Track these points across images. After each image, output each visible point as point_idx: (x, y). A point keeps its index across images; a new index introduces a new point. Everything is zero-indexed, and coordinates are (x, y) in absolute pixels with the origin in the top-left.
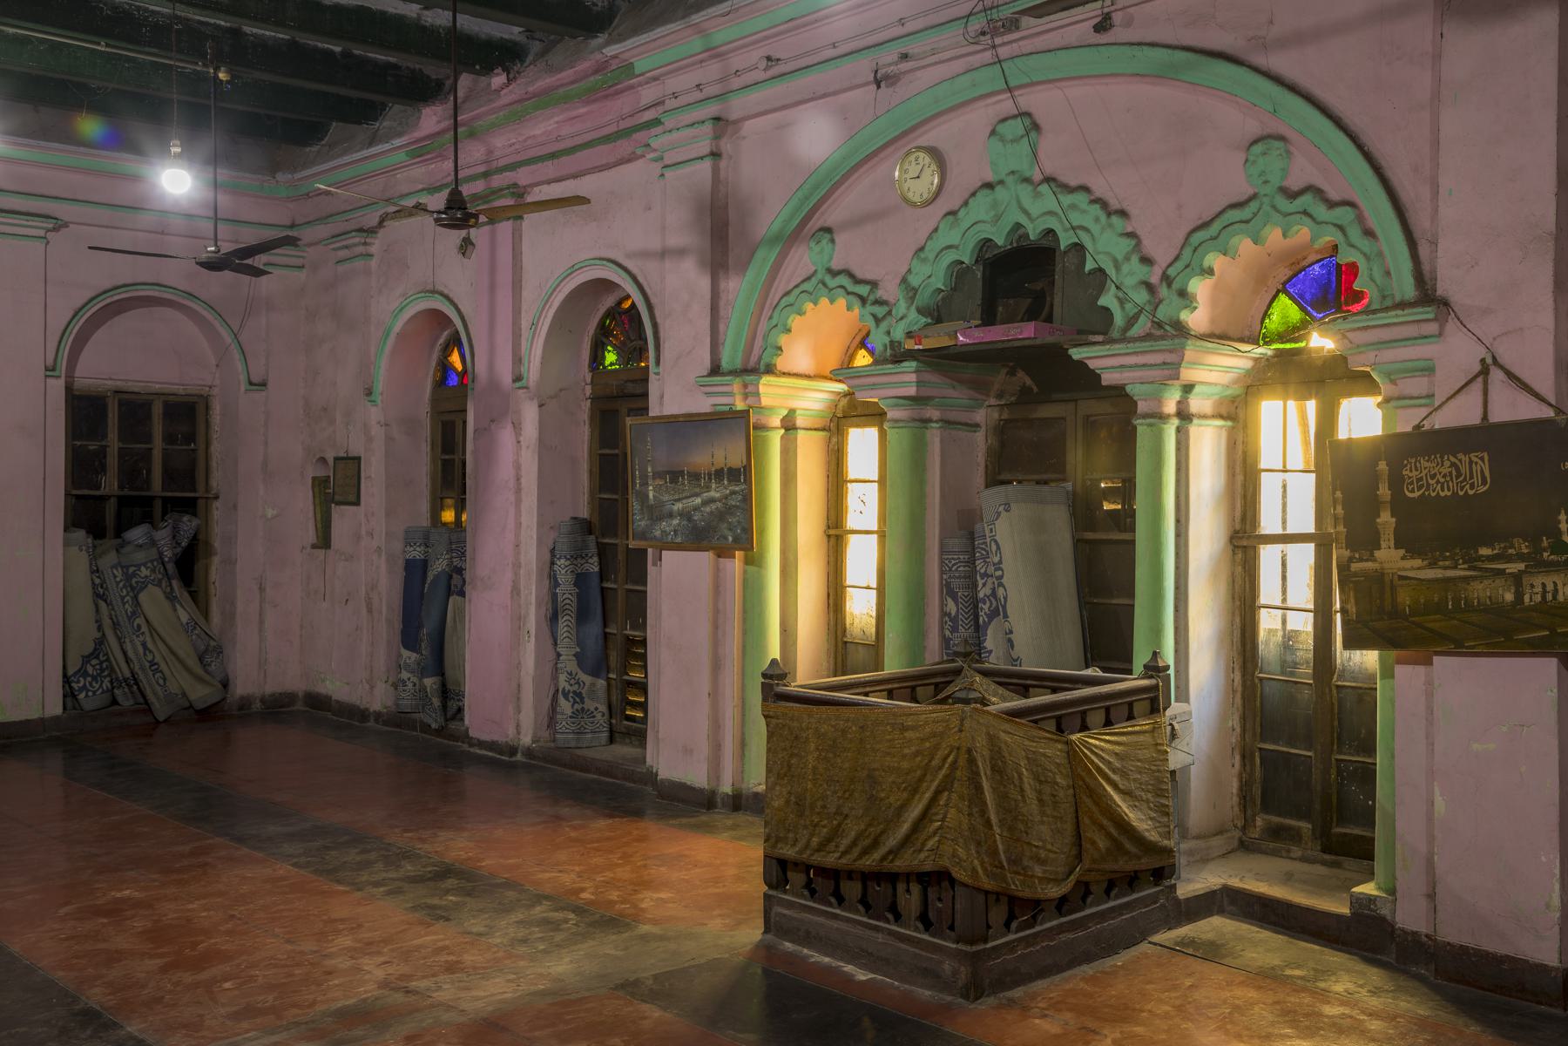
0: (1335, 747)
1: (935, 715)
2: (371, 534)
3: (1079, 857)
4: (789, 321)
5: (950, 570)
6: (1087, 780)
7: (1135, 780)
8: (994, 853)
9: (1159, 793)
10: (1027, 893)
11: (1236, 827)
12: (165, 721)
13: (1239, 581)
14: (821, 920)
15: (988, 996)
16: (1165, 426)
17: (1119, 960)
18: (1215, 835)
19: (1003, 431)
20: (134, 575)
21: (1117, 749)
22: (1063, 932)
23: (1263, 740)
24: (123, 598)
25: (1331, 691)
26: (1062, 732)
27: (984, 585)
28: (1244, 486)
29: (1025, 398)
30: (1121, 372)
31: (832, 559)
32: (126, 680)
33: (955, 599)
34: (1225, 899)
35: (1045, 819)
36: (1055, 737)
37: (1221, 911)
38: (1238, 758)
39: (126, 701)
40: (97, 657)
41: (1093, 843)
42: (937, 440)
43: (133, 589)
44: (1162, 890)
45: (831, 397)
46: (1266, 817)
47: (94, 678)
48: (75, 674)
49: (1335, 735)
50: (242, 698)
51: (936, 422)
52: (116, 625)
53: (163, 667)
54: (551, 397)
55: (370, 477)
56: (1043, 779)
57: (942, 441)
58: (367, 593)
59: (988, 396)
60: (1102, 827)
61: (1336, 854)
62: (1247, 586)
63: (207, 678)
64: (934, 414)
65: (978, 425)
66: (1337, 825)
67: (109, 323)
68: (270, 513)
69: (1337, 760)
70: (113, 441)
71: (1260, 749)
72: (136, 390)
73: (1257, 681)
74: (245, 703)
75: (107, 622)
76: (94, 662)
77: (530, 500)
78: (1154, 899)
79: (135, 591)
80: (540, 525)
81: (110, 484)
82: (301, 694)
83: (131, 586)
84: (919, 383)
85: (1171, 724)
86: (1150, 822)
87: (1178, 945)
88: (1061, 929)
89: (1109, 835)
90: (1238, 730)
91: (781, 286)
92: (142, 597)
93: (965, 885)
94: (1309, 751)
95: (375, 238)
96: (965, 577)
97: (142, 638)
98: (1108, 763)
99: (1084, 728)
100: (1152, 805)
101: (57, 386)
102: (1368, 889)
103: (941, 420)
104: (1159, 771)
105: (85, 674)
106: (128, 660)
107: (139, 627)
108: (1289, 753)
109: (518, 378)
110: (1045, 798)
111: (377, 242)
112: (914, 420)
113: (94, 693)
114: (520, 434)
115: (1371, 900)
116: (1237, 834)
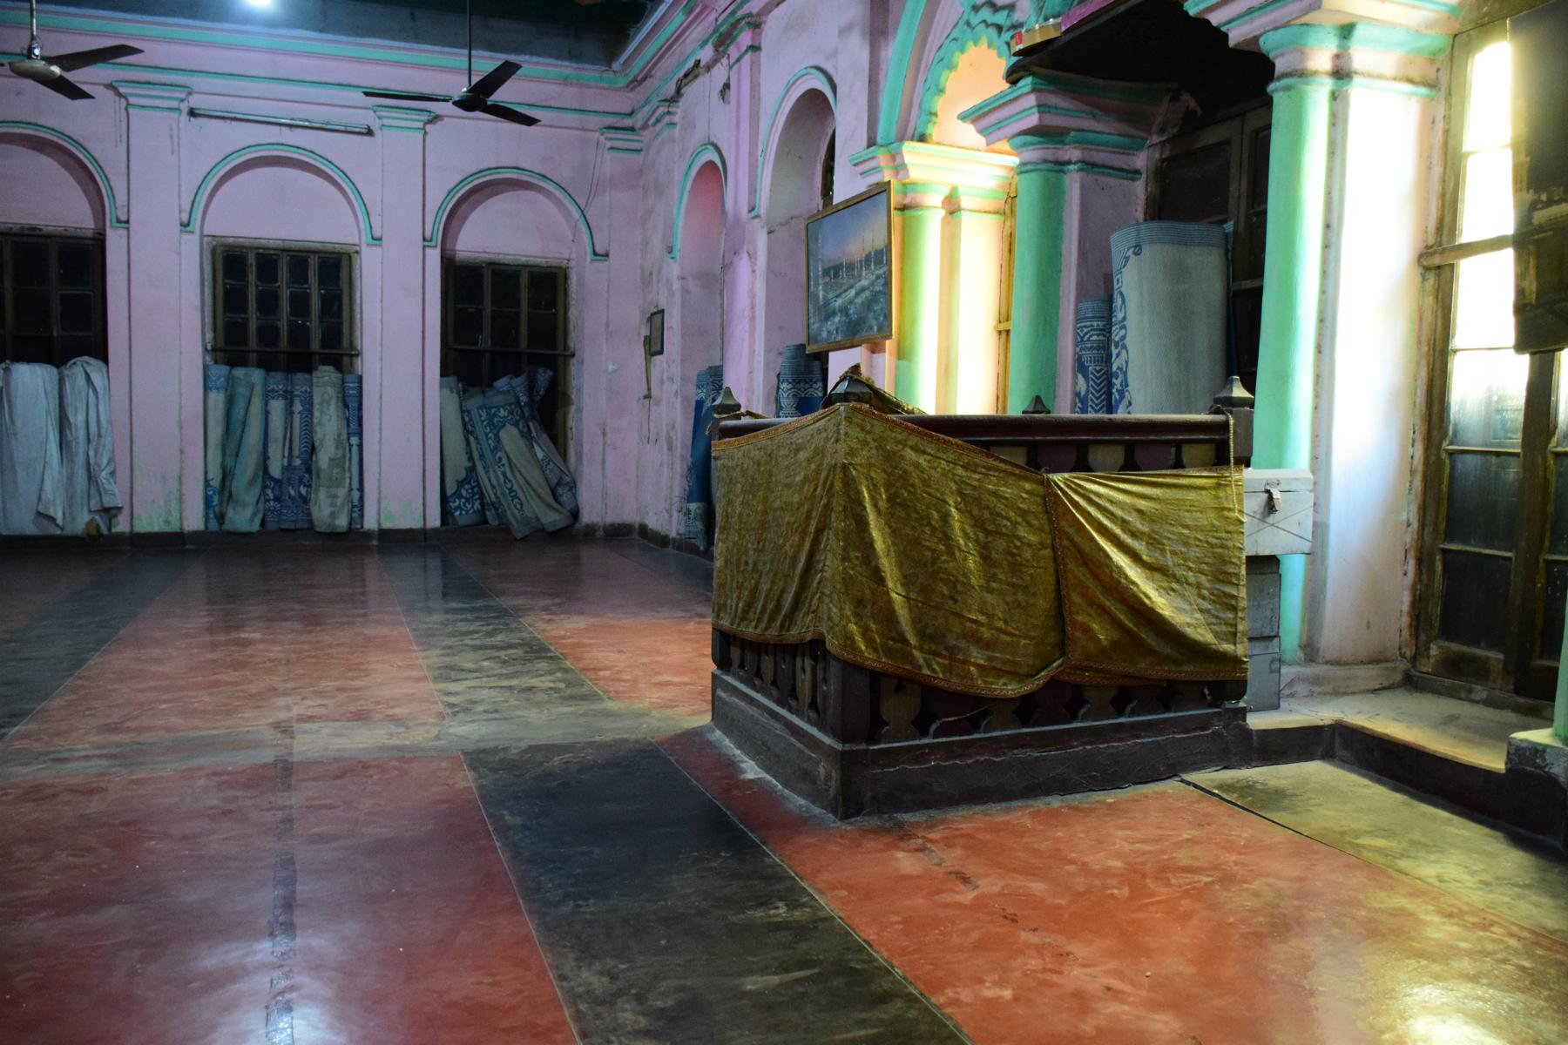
0: (1547, 543)
1: (817, 425)
2: (671, 379)
3: (1062, 647)
4: (942, 80)
5: (1082, 341)
6: (1077, 539)
7: (1173, 553)
8: (889, 617)
9: (1221, 577)
10: (955, 684)
11: (1403, 656)
12: (522, 539)
13: (1428, 317)
14: (742, 704)
15: (870, 814)
16: (1304, 87)
17: (1110, 797)
18: (1363, 663)
19: (1163, 175)
20: (495, 415)
21: (1142, 504)
22: (1022, 746)
23: (1450, 538)
24: (486, 434)
25: (1545, 460)
26: (1039, 468)
27: (1118, 355)
28: (1444, 181)
29: (1191, 125)
30: (1251, 21)
31: (1002, 358)
32: (493, 504)
33: (1086, 377)
34: (1338, 740)
35: (994, 585)
36: (1023, 473)
37: (1328, 756)
38: (1412, 562)
39: (493, 522)
40: (469, 483)
41: (1087, 630)
42: (1076, 187)
43: (495, 427)
44: (1219, 713)
45: (1002, 173)
46: (1446, 644)
47: (467, 500)
48: (452, 496)
49: (1548, 526)
50: (587, 526)
51: (1075, 163)
52: (482, 457)
53: (520, 494)
54: (782, 224)
55: (671, 328)
56: (991, 527)
57: (1083, 187)
58: (668, 433)
59: (1149, 132)
60: (1104, 611)
61: (1535, 697)
62: (1439, 324)
63: (556, 506)
64: (1074, 154)
65: (1138, 172)
66: (1541, 657)
67: (483, 204)
68: (611, 367)
69: (1549, 563)
70: (488, 306)
71: (1444, 551)
72: (506, 262)
73: (1444, 455)
74: (590, 531)
75: (476, 454)
76: (467, 487)
77: (760, 326)
78: (1204, 723)
79: (497, 428)
80: (768, 350)
81: (485, 341)
82: (637, 526)
83: (493, 424)
84: (1041, 106)
85: (1268, 492)
86: (1198, 615)
87: (1217, 788)
88: (1015, 742)
89: (1116, 623)
90: (1415, 525)
91: (935, 39)
92: (503, 434)
93: (837, 659)
94: (1510, 551)
95: (678, 107)
96: (1098, 348)
97: (502, 469)
98: (1123, 523)
99: (1082, 465)
100: (1205, 592)
101: (434, 256)
102: (1539, 736)
103: (1080, 162)
104: (1222, 546)
105: (460, 496)
106: (493, 487)
107: (500, 458)
108: (1480, 554)
109: (752, 209)
110: (994, 555)
111: (679, 111)
112: (1046, 161)
113: (467, 512)
114: (755, 264)
115: (1538, 750)
116: (1403, 665)
